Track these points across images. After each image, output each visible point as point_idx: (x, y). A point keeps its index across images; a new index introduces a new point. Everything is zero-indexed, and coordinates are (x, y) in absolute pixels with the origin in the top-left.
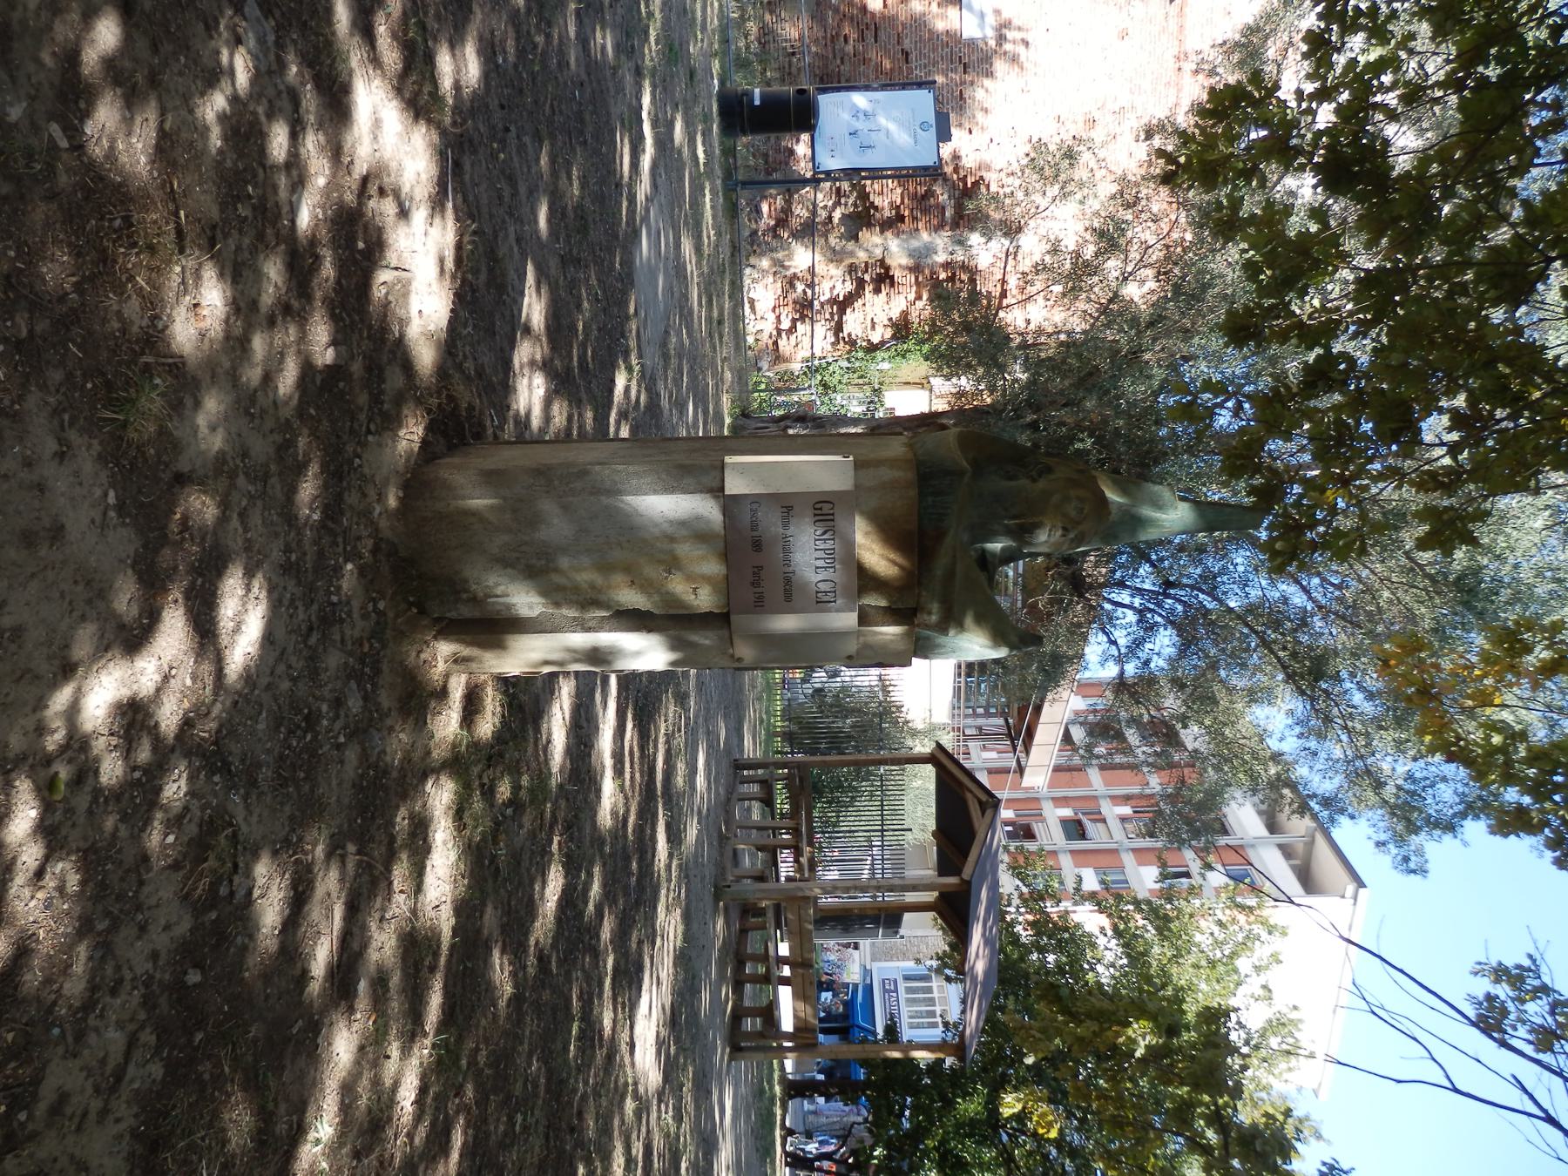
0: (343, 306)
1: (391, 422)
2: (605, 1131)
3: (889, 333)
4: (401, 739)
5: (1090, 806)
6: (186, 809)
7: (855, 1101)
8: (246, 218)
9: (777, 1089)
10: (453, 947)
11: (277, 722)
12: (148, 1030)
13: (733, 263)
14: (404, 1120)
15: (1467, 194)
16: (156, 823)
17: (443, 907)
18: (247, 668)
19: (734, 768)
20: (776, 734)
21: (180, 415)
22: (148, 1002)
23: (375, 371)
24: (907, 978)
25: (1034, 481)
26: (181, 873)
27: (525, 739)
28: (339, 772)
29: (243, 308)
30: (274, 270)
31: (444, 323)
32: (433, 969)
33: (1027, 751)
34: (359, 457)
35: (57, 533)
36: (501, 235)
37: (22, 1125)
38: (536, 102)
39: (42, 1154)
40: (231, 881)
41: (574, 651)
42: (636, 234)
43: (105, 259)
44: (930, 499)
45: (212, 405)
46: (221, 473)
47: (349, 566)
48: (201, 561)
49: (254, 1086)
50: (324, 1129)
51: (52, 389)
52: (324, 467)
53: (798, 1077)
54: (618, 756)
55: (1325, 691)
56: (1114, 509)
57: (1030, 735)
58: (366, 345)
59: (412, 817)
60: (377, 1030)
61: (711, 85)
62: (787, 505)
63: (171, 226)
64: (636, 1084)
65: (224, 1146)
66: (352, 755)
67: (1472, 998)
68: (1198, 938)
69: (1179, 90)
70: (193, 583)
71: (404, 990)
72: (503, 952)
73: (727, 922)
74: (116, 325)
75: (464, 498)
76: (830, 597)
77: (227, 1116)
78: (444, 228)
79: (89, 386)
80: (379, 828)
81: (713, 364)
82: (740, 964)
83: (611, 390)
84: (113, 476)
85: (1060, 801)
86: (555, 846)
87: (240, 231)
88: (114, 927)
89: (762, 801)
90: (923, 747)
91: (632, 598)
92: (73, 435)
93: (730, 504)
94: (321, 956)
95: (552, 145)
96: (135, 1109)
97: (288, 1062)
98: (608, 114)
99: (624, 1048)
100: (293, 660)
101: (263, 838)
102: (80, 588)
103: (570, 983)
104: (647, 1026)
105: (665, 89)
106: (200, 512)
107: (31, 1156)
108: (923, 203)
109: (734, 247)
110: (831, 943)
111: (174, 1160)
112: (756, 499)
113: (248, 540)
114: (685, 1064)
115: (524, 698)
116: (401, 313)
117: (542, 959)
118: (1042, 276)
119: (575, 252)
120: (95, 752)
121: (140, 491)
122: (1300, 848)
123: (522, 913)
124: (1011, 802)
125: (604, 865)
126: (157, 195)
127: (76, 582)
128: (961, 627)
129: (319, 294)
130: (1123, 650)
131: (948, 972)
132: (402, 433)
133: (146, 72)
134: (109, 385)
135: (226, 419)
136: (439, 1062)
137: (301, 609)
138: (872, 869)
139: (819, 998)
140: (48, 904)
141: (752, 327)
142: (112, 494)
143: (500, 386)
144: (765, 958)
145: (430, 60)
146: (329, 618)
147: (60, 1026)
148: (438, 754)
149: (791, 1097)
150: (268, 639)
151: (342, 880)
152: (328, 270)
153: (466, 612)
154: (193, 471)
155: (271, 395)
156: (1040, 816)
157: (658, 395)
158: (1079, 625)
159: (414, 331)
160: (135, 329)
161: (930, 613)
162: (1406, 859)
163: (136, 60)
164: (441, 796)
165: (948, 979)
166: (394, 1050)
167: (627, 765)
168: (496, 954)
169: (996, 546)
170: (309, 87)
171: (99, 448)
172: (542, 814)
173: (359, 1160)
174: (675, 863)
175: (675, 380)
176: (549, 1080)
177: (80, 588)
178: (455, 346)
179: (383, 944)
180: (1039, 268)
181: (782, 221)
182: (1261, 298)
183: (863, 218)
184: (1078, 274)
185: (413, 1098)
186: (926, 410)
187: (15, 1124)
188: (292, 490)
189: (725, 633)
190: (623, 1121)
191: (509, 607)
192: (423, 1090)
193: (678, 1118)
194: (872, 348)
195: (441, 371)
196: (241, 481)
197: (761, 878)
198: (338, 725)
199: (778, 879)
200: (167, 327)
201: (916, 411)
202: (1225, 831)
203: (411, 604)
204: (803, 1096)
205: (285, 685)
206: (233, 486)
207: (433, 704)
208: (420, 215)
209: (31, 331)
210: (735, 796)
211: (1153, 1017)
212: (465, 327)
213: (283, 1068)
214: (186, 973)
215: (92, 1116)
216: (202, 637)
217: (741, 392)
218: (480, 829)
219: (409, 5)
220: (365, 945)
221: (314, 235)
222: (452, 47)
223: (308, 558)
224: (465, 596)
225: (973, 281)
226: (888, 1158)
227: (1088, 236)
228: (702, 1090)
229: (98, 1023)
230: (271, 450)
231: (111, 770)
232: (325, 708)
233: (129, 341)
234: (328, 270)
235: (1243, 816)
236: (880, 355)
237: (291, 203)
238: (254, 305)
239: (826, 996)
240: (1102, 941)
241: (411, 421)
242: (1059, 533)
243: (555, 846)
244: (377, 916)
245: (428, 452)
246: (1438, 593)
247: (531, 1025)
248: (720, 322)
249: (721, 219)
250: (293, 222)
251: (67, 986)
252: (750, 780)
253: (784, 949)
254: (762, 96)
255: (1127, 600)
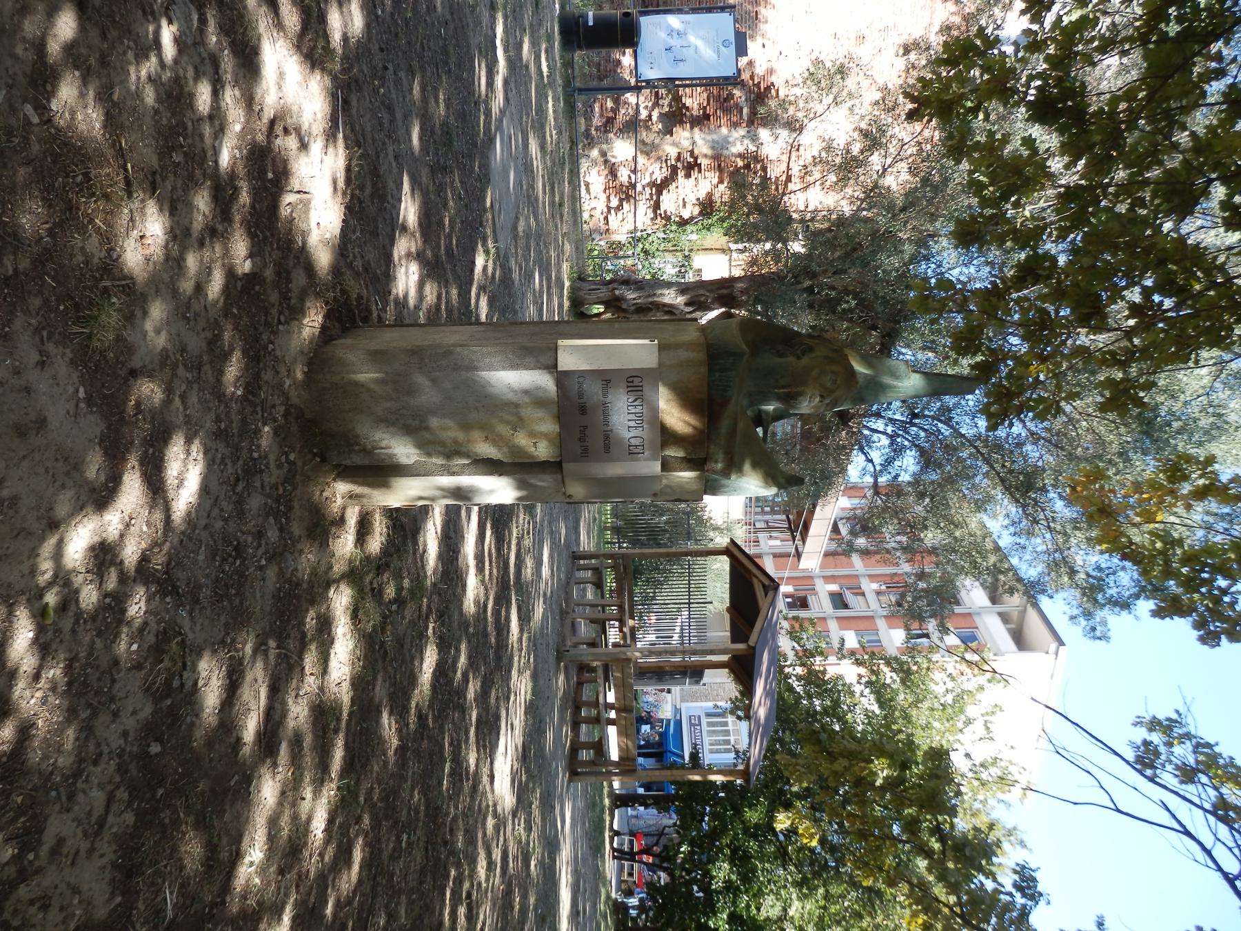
0: (257, 226)
1: (297, 313)
2: (471, 841)
3: (697, 211)
4: (308, 557)
5: (852, 583)
6: (146, 624)
7: (667, 810)
8: (179, 163)
9: (607, 802)
10: (350, 714)
11: (213, 553)
12: (122, 789)
13: (571, 155)
14: (317, 844)
15: (817, 702)
16: (123, 636)
17: (344, 684)
18: (189, 513)
19: (572, 558)
20: (606, 529)
21: (132, 325)
22: (122, 769)
23: (283, 274)
24: (709, 715)
25: (799, 358)
26: (143, 672)
27: (406, 551)
28: (262, 587)
29: (179, 236)
30: (202, 202)
31: (337, 231)
32: (336, 731)
33: (804, 540)
34: (273, 343)
35: (41, 423)
36: (382, 155)
37: (31, 862)
38: (409, 43)
39: (46, 883)
40: (181, 676)
41: (442, 489)
42: (491, 140)
43: (71, 208)
44: (717, 374)
45: (157, 311)
46: (165, 366)
47: (267, 429)
48: (151, 435)
49: (202, 824)
50: (255, 854)
51: (34, 313)
52: (245, 352)
53: (624, 792)
54: (479, 558)
55: (1035, 500)
56: (860, 380)
57: (806, 528)
58: (276, 254)
59: (318, 617)
60: (294, 780)
61: (554, 9)
62: (606, 378)
63: (121, 176)
64: (495, 805)
65: (181, 871)
66: (271, 573)
67: (1132, 744)
68: (932, 686)
69: (933, 13)
70: (146, 452)
71: (315, 748)
72: (391, 714)
73: (567, 678)
74: (81, 258)
75: (355, 372)
76: (639, 450)
77: (183, 850)
78: (336, 155)
79: (62, 308)
80: (293, 627)
81: (556, 240)
82: (577, 709)
83: (472, 270)
84: (82, 376)
85: (829, 579)
86: (430, 631)
87: (175, 174)
88: (94, 715)
89: (594, 584)
90: (722, 541)
91: (486, 450)
92: (50, 347)
93: (562, 379)
94: (250, 727)
95: (423, 77)
96: (114, 847)
97: (228, 807)
98: (469, 46)
99: (485, 779)
100: (224, 504)
101: (205, 641)
102: (60, 464)
103: (443, 733)
104: (504, 764)
105: (515, 19)
106: (150, 398)
107: (38, 885)
108: (725, 105)
109: (572, 142)
110: (649, 689)
111: (144, 883)
112: (583, 374)
113: (186, 416)
114: (534, 788)
115: (404, 520)
116: (303, 226)
117: (421, 717)
118: (819, 167)
119: (442, 161)
120: (76, 585)
121: (103, 386)
122: (1015, 615)
123: (405, 683)
124: (790, 580)
125: (469, 642)
126: (109, 153)
127: (57, 460)
128: (740, 470)
129: (237, 218)
130: (878, 468)
131: (740, 713)
132: (306, 321)
133: (97, 56)
134: (76, 306)
135: (168, 323)
136: (343, 799)
137: (230, 465)
138: (682, 637)
139: (638, 731)
140: (44, 701)
141: (586, 206)
142: (82, 390)
143: (383, 275)
144: (596, 704)
145: (322, 19)
146: (251, 470)
147: (57, 790)
148: (338, 568)
149: (617, 807)
150: (205, 489)
151: (265, 669)
152: (245, 197)
153: (357, 460)
154: (144, 366)
155: (202, 301)
156: (813, 590)
157: (510, 270)
158: (844, 447)
159: (314, 239)
160: (96, 260)
161: (716, 462)
162: (1094, 629)
163: (89, 47)
164: (341, 600)
165: (739, 718)
166: (308, 793)
167: (487, 564)
168: (385, 715)
169: (770, 408)
170: (226, 52)
171: (70, 355)
172: (420, 607)
173: (283, 876)
174: (525, 636)
175: (524, 256)
176: (427, 808)
177: (60, 464)
178: (346, 250)
179: (298, 712)
180: (816, 161)
181: (609, 122)
182: (982, 209)
183: (676, 117)
184: (848, 167)
185: (323, 827)
186: (726, 275)
187: (26, 862)
188: (221, 373)
189: (559, 476)
190: (485, 834)
191: (392, 456)
192: (330, 821)
193: (529, 829)
194: (683, 223)
195: (336, 270)
196: (181, 371)
197: (593, 644)
198: (260, 552)
199: (606, 646)
200: (120, 256)
201: (718, 277)
202: (958, 603)
203: (315, 455)
204: (627, 806)
205: (219, 524)
206: (174, 375)
207: (333, 530)
208: (317, 146)
209: (15, 270)
210: (573, 580)
211: (890, 756)
212: (354, 232)
213: (224, 811)
214: (149, 746)
215: (83, 854)
216: (154, 494)
217: (578, 259)
218: (372, 622)
219: (262, 926)
220: (284, 714)
221: (233, 171)
222: (340, 5)
223: (234, 425)
224: (357, 448)
225: (764, 169)
226: (692, 853)
227: (856, 135)
228: (548, 806)
229: (84, 786)
230: (204, 344)
231: (89, 596)
232: (250, 539)
233: (91, 270)
234: (245, 197)
235: (974, 595)
236: (689, 228)
237: (214, 148)
238: (187, 232)
239: (646, 728)
240: (858, 689)
241: (313, 312)
242: (818, 399)
243: (430, 631)
244: (293, 694)
245: (327, 337)
246: (1125, 425)
247: (413, 767)
248: (561, 205)
249: (562, 120)
250: (216, 162)
251: (61, 760)
252: (585, 568)
253: (611, 697)
254: (595, 18)
255: (881, 428)
